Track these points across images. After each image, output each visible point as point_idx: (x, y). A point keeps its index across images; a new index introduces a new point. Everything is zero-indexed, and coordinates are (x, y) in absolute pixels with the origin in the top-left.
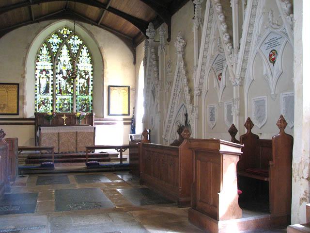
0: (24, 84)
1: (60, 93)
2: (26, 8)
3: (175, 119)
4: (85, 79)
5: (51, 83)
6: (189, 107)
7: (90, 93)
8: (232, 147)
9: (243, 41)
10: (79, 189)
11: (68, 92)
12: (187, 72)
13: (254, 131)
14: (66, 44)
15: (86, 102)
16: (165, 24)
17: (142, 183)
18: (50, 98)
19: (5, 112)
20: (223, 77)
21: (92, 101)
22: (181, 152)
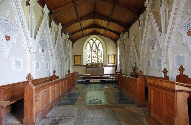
0: (82, 55)
1: (93, 57)
2: (81, 31)
3: (132, 65)
5: (91, 55)
6: (137, 61)
7: (103, 57)
8: (184, 87)
9: (169, 29)
11: (96, 57)
12: (136, 48)
13: (184, 73)
14: (95, 43)
16: (127, 32)
17: (120, 89)
18: (91, 59)
19: (77, 64)
20: (155, 48)
22: (138, 81)
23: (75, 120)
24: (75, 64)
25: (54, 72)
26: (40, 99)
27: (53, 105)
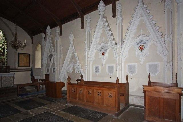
4: (2, 48)
10: (34, 116)
15: (3, 60)
21: (6, 60)
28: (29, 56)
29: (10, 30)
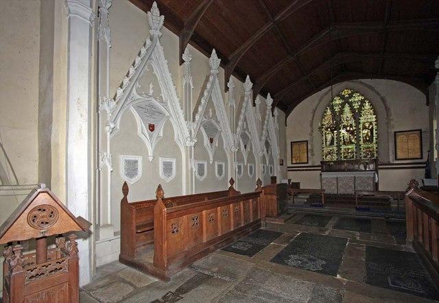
7: (375, 141)
18: (335, 149)
19: (298, 161)
23: (233, 286)
24: (292, 164)
25: (232, 181)
26: (181, 231)
27: (212, 247)
28: (421, 135)
29: (378, 93)
